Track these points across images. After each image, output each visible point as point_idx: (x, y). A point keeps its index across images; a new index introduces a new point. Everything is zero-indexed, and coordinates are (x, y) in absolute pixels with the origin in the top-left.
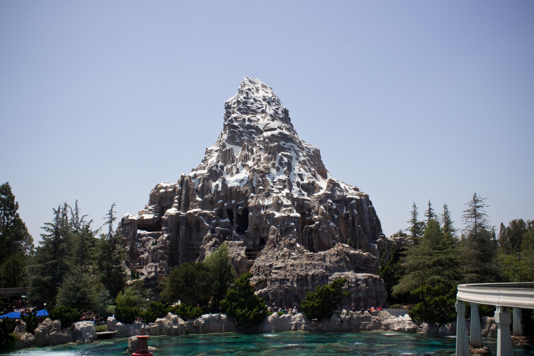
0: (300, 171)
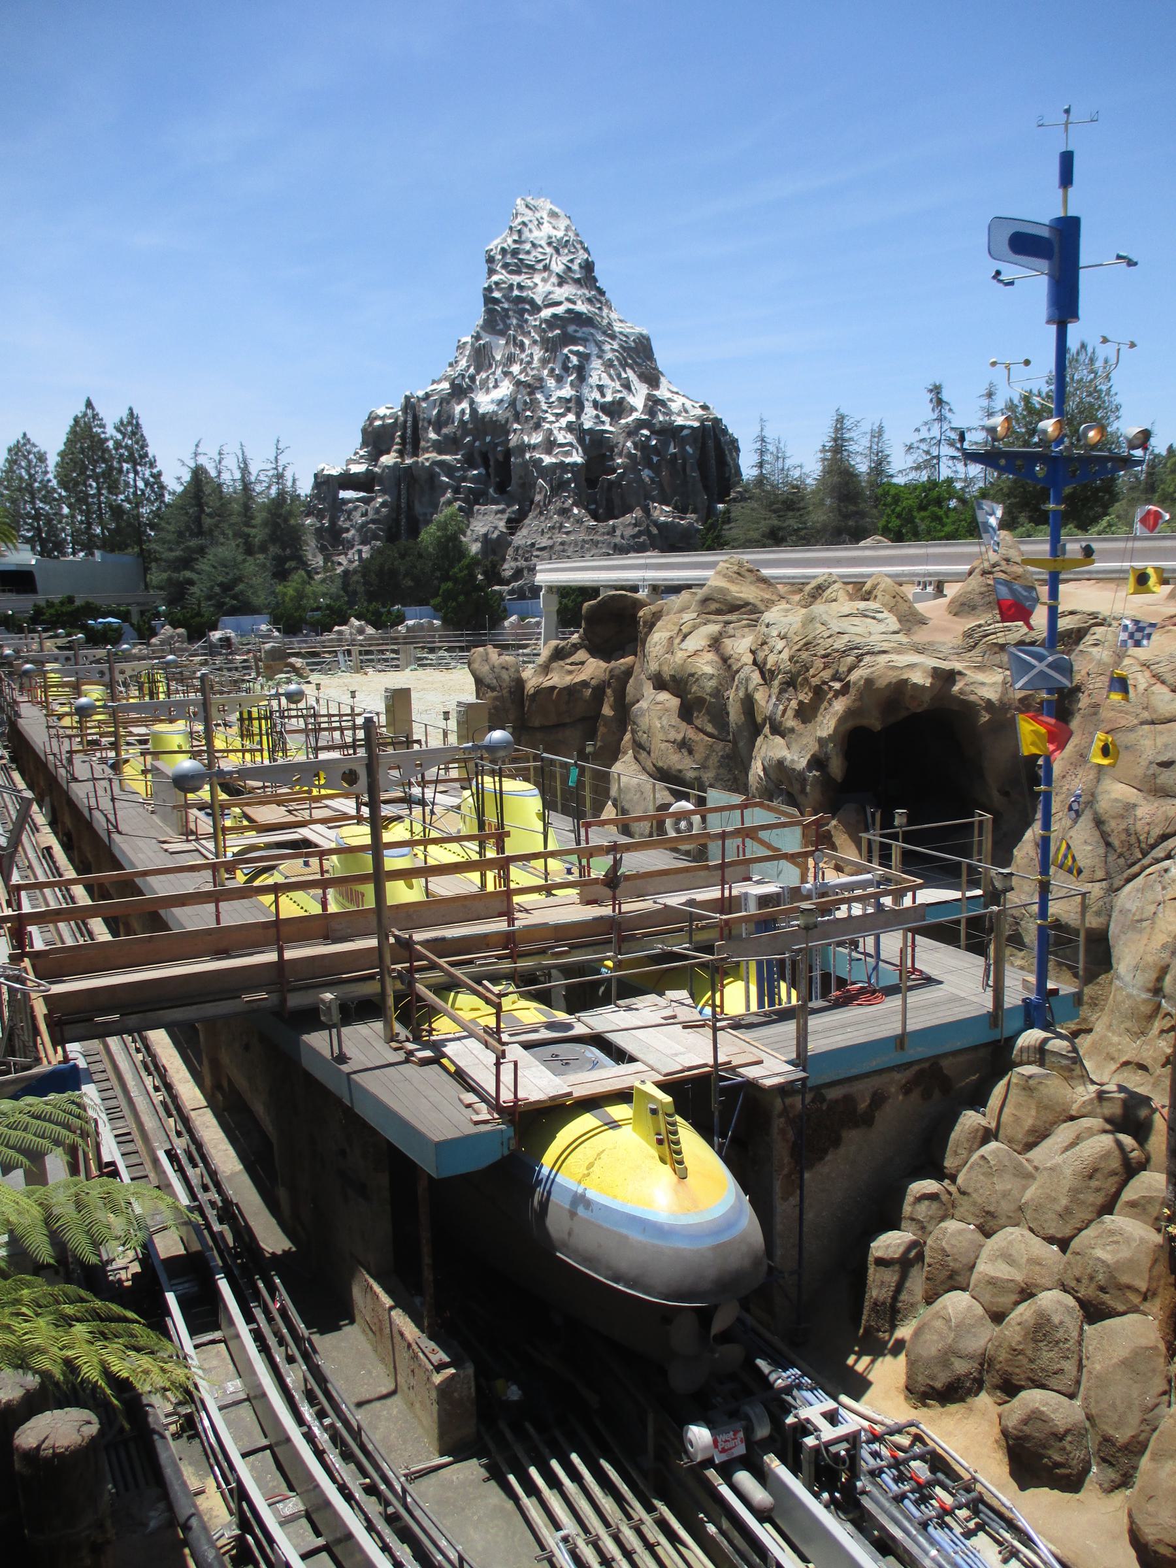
0: (600, 379)
